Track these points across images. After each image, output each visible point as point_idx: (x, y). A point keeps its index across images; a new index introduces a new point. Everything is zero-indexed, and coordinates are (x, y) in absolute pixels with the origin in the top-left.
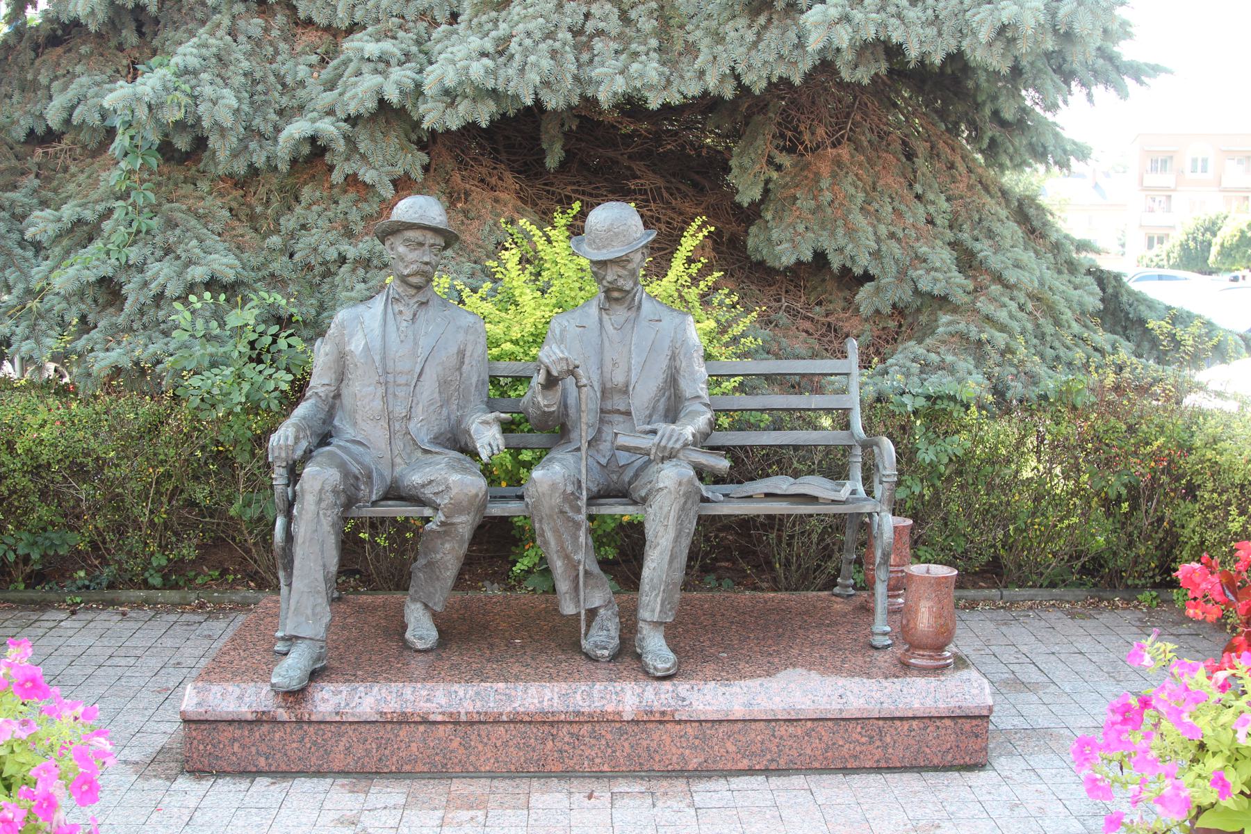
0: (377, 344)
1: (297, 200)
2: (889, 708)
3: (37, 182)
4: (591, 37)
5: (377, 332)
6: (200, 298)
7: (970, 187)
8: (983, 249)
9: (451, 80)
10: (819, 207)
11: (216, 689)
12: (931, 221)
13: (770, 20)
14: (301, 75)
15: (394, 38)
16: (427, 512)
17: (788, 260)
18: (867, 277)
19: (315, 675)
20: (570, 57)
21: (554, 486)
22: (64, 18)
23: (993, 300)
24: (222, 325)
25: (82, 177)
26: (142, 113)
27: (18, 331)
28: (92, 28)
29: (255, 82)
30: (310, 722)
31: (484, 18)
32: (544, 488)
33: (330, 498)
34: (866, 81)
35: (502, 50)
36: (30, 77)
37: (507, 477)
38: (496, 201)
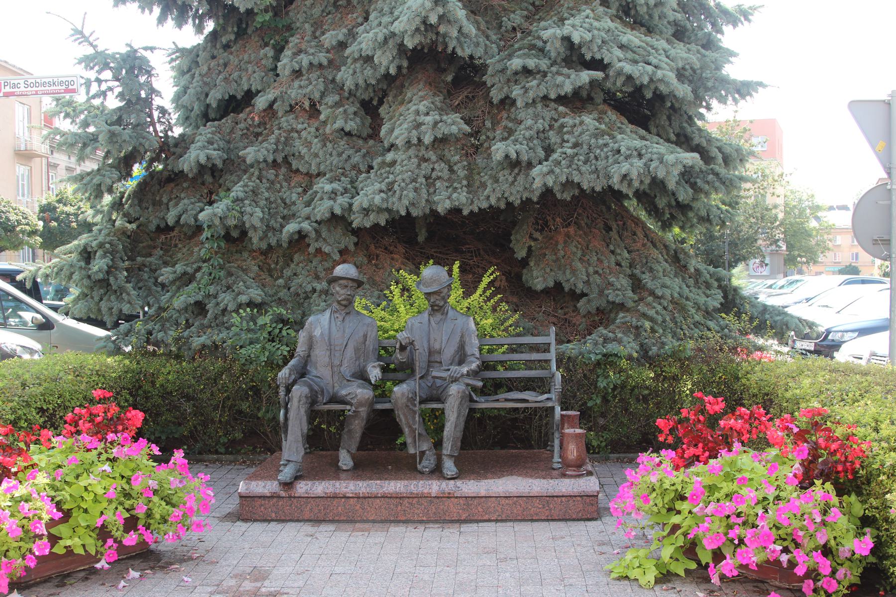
0: (327, 332)
1: (292, 261)
2: (551, 492)
3: (161, 252)
4: (435, 180)
5: (327, 327)
6: (245, 311)
7: (644, 245)
8: (646, 278)
9: (365, 205)
10: (558, 259)
11: (253, 483)
12: (618, 264)
13: (520, 171)
14: (294, 199)
15: (339, 180)
16: (348, 407)
17: (539, 287)
18: (584, 295)
19: (297, 478)
20: (424, 191)
21: (403, 394)
22: (176, 170)
23: (648, 305)
24: (255, 324)
25: (185, 250)
26: (217, 222)
27: (156, 327)
28: (190, 176)
29: (271, 203)
30: (295, 497)
31: (383, 171)
32: (399, 395)
33: (304, 400)
34: (569, 199)
35: (390, 188)
36: (158, 198)
37: (381, 391)
38: (393, 259)
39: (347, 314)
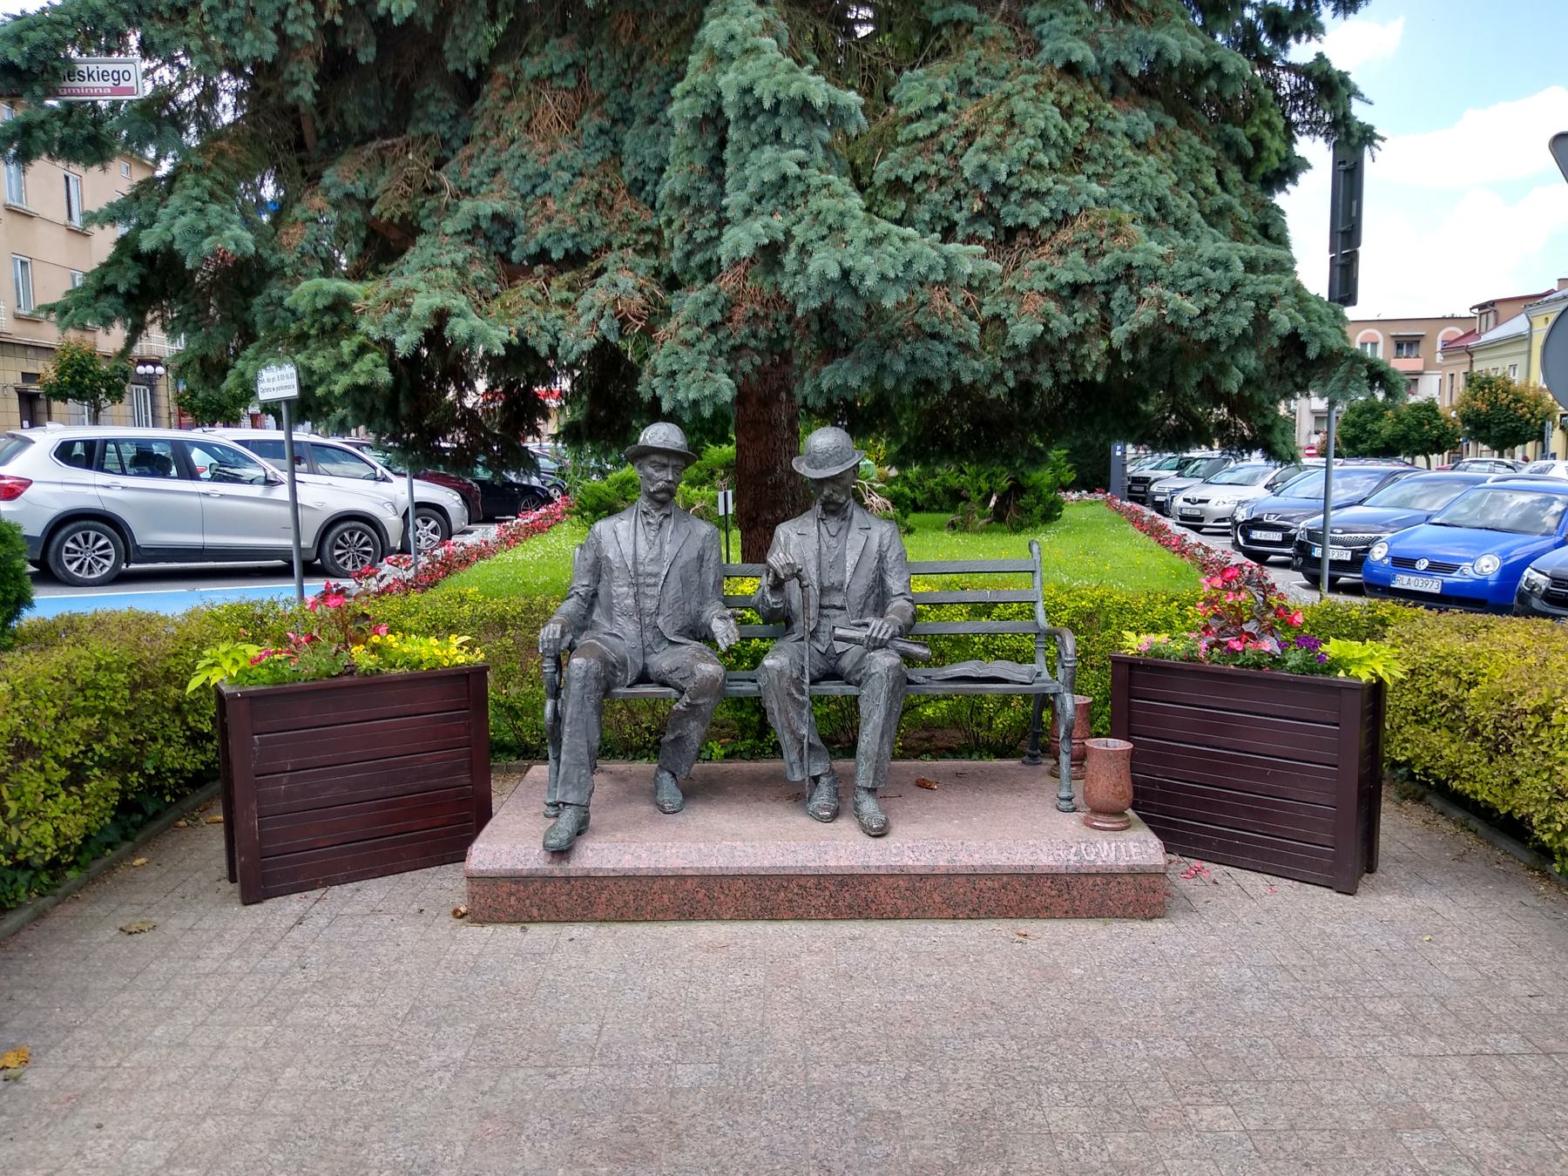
33: (593, 684)
39: (667, 516)
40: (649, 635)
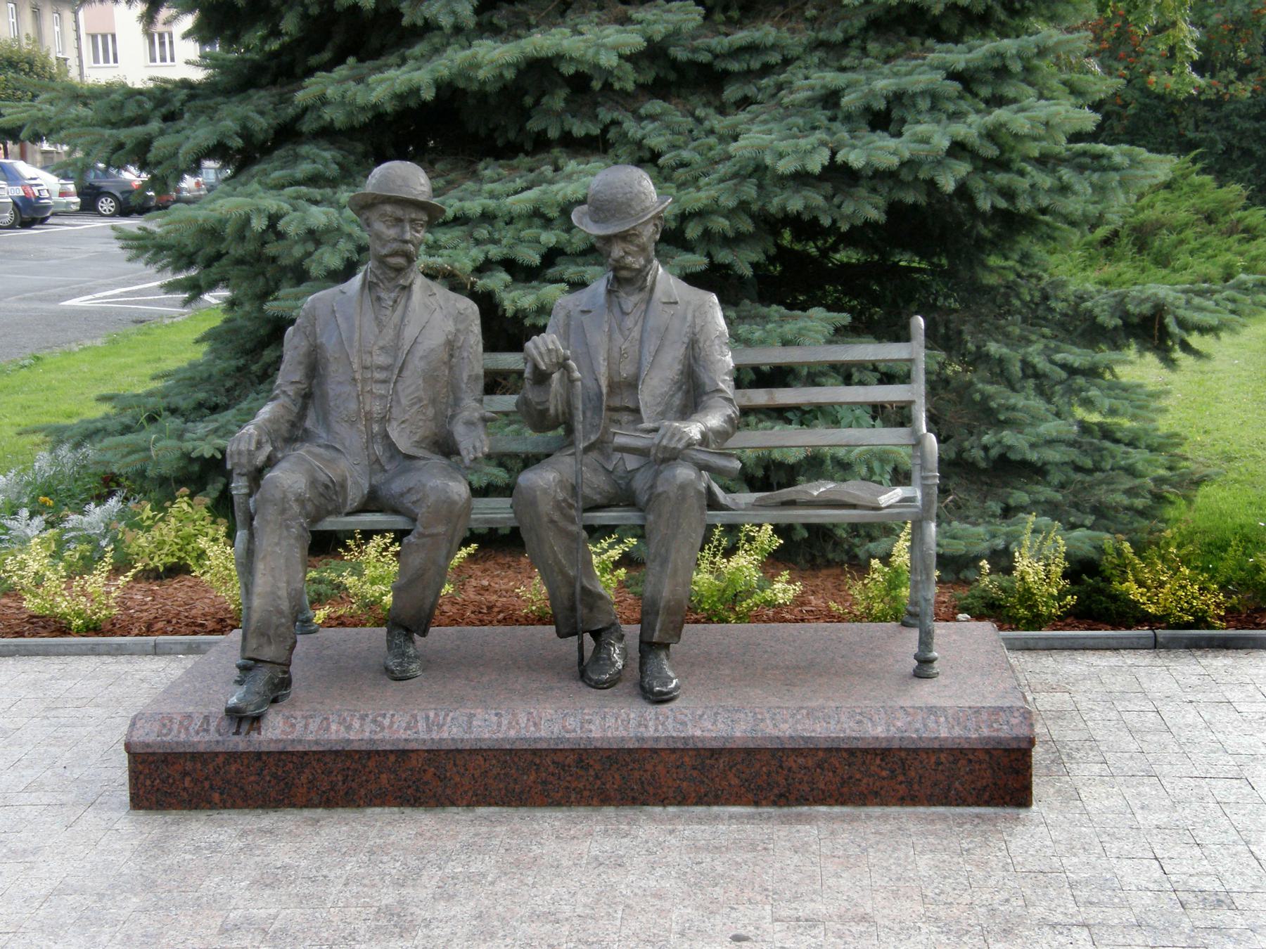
40: (378, 449)
